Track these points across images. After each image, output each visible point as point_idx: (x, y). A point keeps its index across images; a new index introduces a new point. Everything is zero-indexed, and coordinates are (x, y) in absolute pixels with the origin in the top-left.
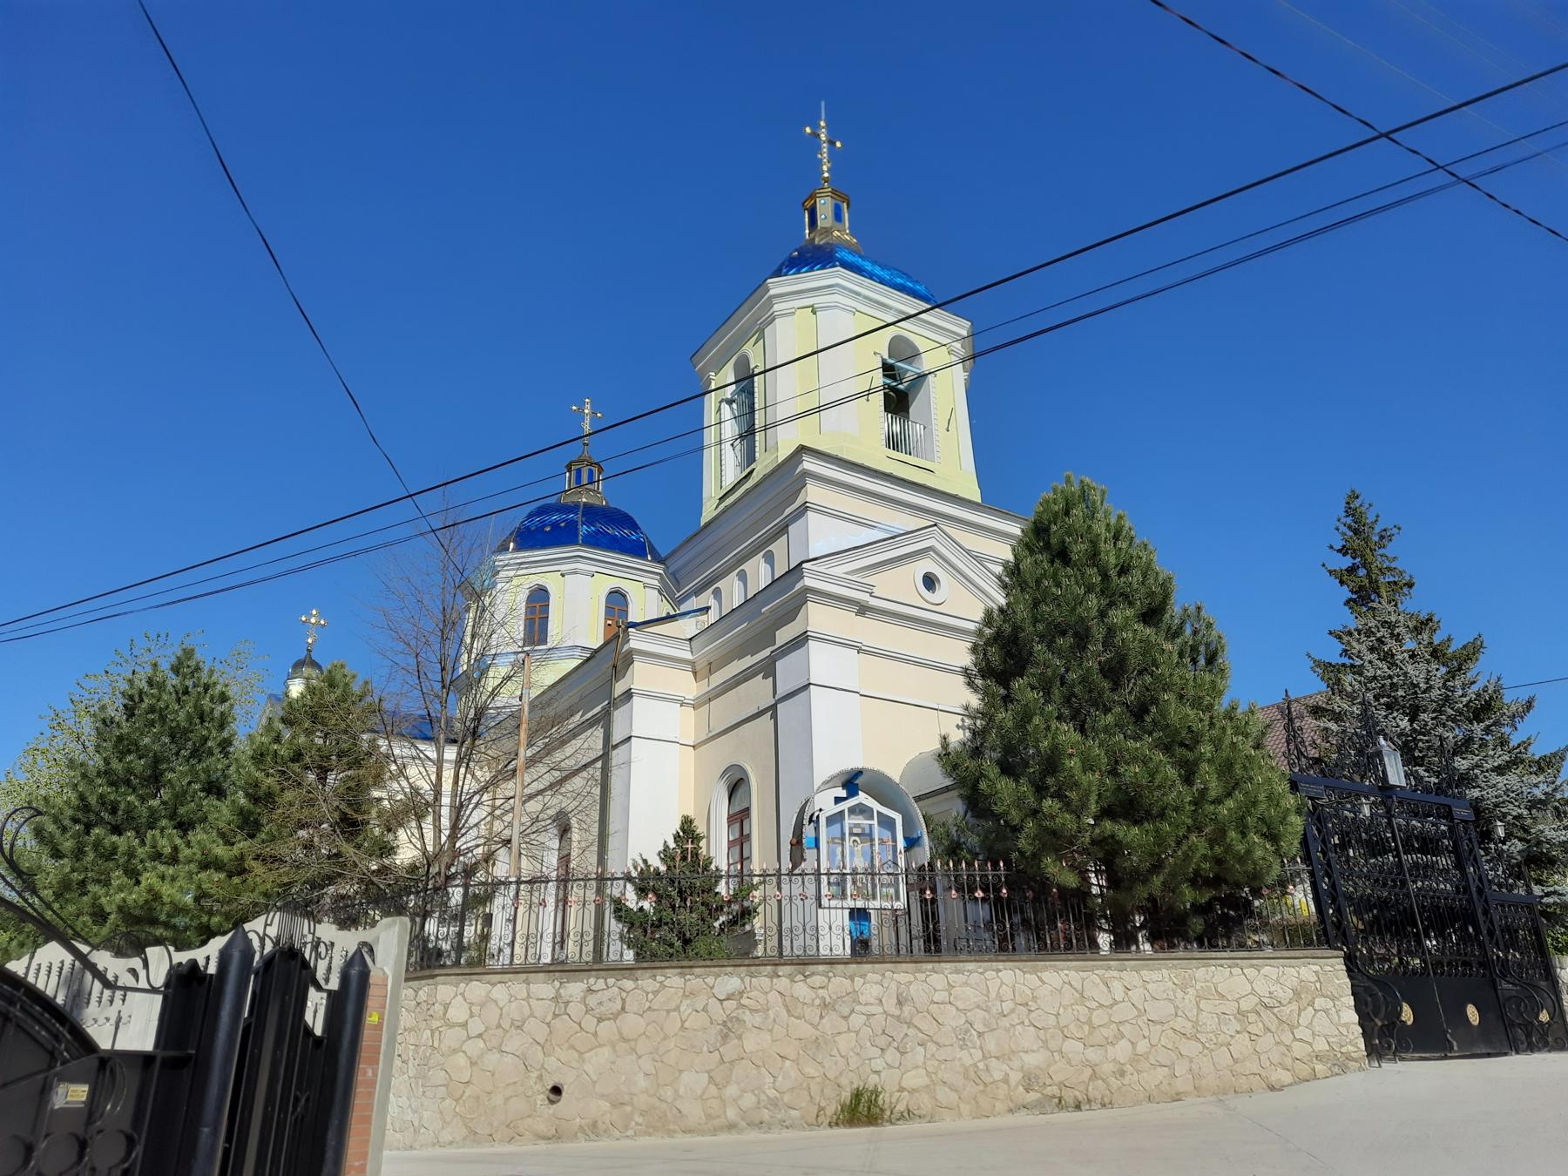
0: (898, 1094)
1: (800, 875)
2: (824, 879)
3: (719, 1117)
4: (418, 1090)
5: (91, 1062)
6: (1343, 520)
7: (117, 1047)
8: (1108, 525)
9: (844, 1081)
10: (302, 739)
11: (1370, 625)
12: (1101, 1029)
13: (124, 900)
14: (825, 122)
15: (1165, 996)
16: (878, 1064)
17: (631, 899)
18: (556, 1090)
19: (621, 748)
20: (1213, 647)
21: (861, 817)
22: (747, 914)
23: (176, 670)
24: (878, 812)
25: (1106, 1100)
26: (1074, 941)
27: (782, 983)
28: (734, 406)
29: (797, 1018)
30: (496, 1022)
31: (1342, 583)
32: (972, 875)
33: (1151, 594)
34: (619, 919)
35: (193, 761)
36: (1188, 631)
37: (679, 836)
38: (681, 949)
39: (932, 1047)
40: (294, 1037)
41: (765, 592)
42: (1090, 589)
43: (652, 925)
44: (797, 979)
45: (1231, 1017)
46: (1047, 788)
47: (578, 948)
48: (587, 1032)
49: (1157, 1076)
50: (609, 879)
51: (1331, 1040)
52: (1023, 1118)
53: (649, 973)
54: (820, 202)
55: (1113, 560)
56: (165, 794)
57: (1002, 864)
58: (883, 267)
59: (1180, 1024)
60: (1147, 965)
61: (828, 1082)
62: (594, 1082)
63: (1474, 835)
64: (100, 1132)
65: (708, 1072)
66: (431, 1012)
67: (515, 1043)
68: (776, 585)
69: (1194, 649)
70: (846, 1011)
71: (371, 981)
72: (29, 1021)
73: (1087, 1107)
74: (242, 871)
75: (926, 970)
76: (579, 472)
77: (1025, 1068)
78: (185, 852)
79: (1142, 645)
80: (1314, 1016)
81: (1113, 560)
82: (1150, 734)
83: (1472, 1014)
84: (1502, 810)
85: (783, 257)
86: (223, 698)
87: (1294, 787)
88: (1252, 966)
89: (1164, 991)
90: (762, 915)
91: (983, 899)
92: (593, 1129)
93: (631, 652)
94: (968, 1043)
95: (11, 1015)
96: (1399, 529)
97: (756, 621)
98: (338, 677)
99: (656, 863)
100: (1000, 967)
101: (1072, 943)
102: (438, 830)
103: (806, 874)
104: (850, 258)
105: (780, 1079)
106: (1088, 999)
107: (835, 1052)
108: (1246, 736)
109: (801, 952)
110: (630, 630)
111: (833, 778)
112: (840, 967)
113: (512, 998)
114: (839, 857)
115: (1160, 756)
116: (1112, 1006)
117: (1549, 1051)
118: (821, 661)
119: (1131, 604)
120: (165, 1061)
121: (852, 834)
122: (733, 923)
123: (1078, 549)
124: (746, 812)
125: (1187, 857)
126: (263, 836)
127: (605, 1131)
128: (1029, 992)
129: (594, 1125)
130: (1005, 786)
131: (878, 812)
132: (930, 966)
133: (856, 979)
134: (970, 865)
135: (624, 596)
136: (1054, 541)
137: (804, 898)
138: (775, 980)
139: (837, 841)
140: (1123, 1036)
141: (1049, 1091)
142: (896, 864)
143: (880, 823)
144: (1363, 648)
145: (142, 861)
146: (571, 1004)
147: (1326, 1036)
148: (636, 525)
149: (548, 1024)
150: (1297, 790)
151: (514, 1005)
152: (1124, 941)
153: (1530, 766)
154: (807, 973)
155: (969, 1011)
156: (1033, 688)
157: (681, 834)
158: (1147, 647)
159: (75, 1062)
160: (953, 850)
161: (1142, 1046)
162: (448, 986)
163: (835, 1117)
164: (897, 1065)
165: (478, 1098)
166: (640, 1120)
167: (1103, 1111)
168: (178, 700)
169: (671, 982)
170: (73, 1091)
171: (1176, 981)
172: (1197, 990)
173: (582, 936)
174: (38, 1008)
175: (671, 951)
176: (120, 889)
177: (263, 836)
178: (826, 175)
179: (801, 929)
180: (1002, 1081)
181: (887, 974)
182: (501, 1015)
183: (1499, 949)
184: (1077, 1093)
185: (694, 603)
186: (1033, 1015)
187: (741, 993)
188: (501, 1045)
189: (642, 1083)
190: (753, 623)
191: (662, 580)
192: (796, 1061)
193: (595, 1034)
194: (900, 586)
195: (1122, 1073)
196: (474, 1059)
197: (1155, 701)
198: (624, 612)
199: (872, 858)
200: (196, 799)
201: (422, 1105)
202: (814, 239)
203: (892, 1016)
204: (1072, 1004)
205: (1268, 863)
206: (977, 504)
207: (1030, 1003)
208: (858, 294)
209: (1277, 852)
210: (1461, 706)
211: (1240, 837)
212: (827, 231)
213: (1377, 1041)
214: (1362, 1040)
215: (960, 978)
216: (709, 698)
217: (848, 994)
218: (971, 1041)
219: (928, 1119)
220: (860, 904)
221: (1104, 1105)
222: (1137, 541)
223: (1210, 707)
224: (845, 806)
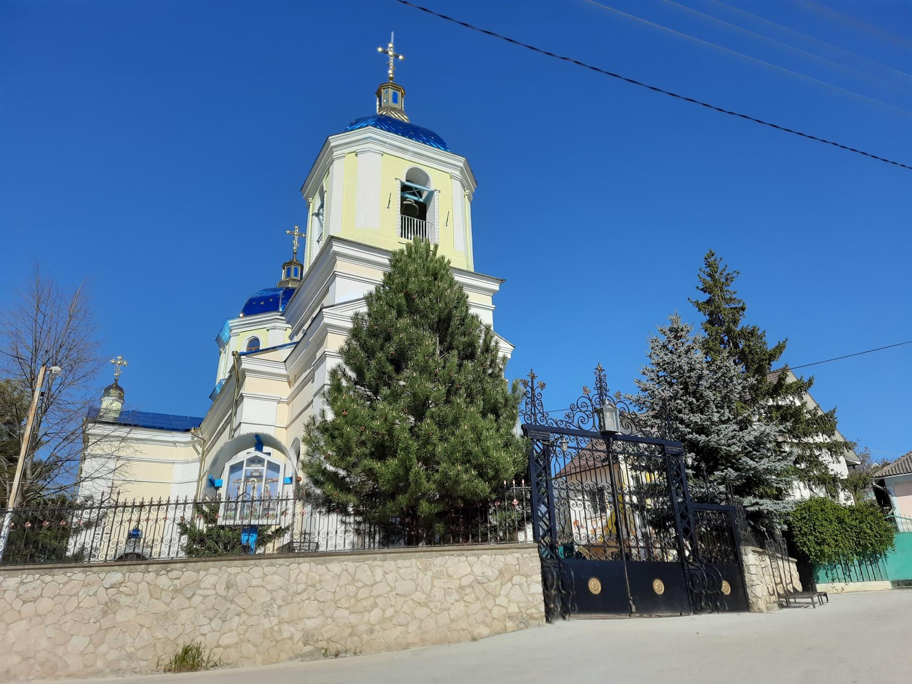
15: (410, 577)
21: (259, 465)
25: (358, 650)
27: (150, 577)
29: (156, 599)
44: (161, 573)
49: (394, 633)
52: (297, 663)
53: (62, 571)
77: (305, 630)
80: (512, 588)
88: (474, 555)
93: (244, 371)
96: (738, 273)
100: (301, 561)
110: (242, 357)
116: (373, 585)
147: (517, 603)
154: (168, 569)
155: (275, 591)
166: (38, 668)
178: (391, 76)
179: (160, 541)
186: (318, 593)
189: (44, 644)
193: (19, 612)
203: (221, 596)
204: (346, 585)
208: (385, 143)
215: (274, 569)
221: (355, 654)
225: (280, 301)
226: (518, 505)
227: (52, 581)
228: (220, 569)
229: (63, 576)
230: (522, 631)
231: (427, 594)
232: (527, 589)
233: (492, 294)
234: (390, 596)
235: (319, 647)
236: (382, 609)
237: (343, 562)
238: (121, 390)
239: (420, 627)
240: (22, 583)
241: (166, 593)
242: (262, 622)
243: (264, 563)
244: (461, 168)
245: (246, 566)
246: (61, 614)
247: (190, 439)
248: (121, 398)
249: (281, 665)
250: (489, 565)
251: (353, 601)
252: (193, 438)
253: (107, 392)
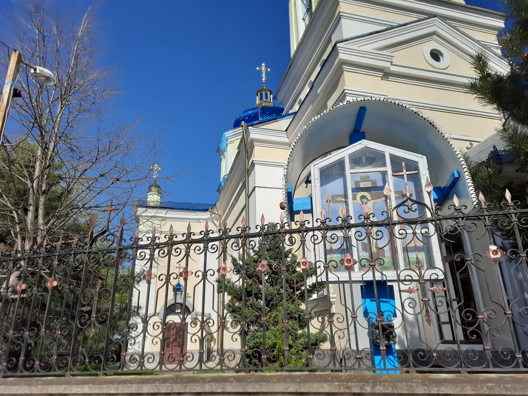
93: (252, 141)
110: (249, 128)
121: (357, 189)
139: (339, 199)
225: (259, 115)
226: (4, 289)
233: (496, 32)
238: (158, 187)
247: (209, 216)
248: (159, 193)
252: (211, 216)
253: (150, 190)
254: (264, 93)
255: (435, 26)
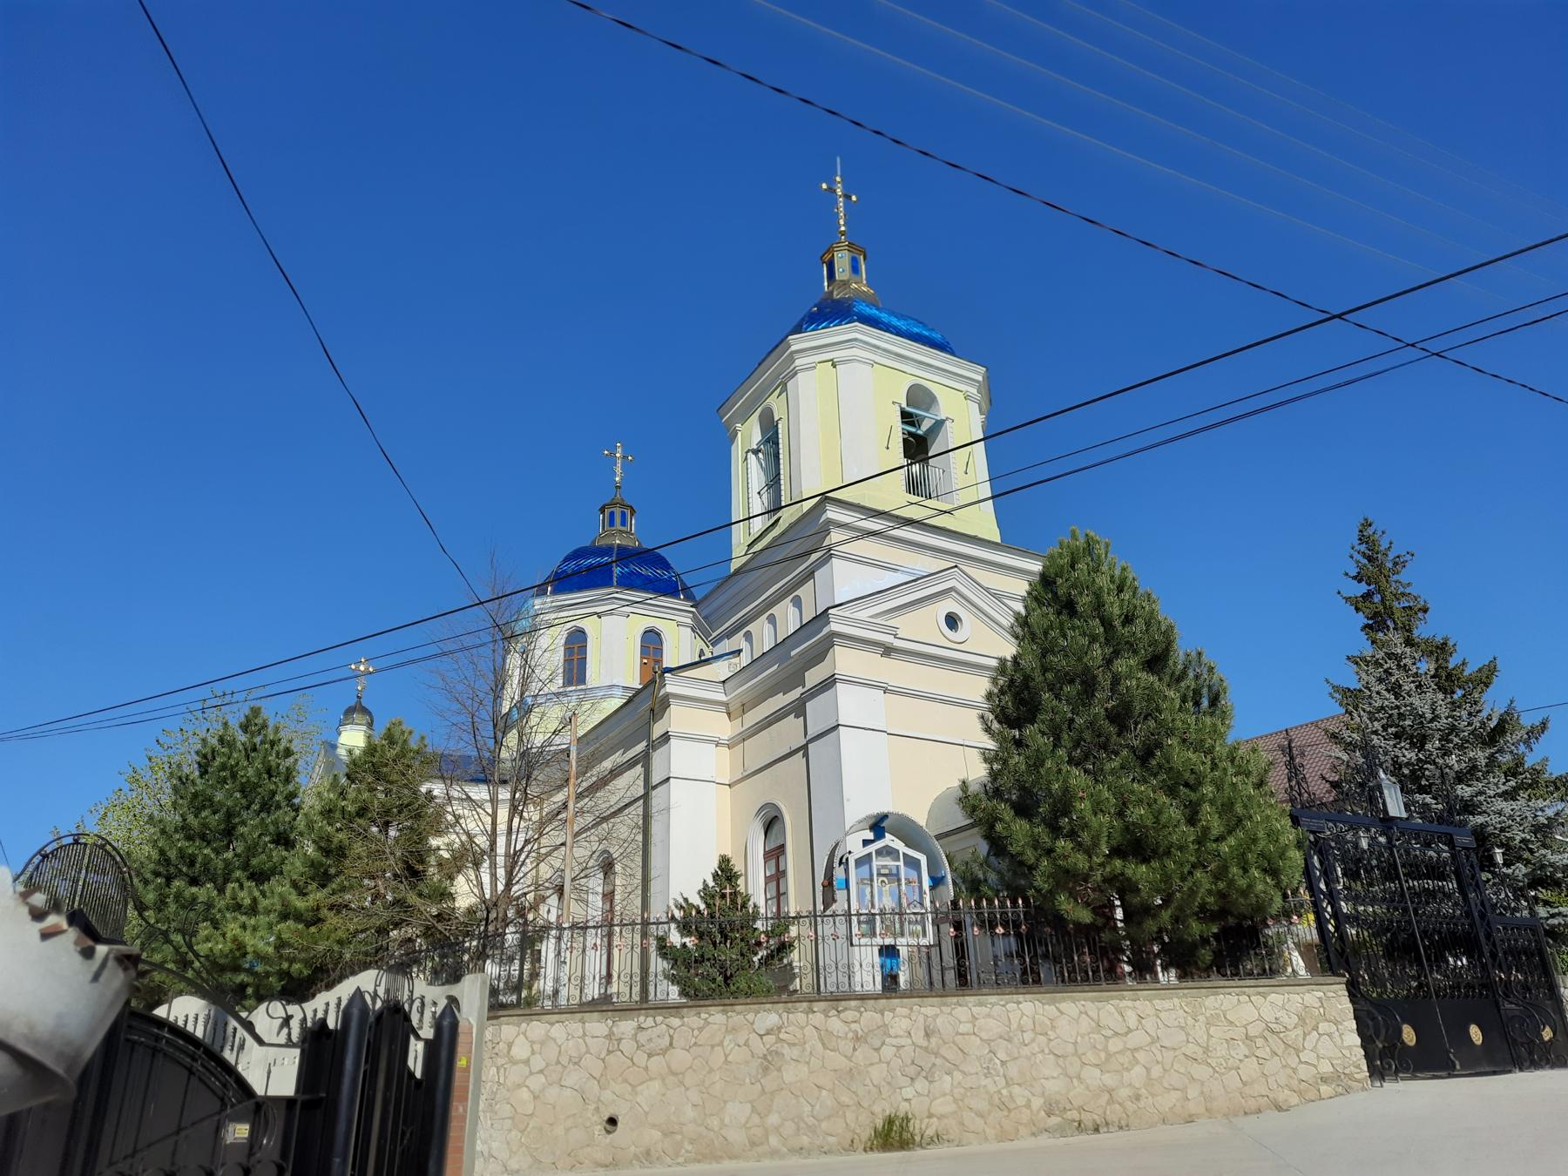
0: (927, 1120)
1: (831, 916)
2: (854, 919)
3: (762, 1144)
4: (486, 1123)
5: (250, 1104)
6: (1357, 548)
7: (269, 1094)
8: (1112, 577)
9: (877, 1109)
10: (366, 795)
11: (1377, 656)
12: (1117, 1055)
13: (211, 950)
14: (841, 176)
15: (1176, 1023)
16: (908, 1092)
17: (675, 938)
18: (612, 1121)
19: (659, 789)
20: (1215, 688)
21: (888, 858)
22: (784, 948)
23: (245, 728)
24: (904, 854)
25: (1123, 1123)
26: (1090, 973)
27: (817, 1018)
28: (760, 455)
29: (831, 1050)
30: (555, 1060)
31: (1357, 609)
32: (992, 913)
33: (1153, 643)
34: (664, 956)
35: (263, 815)
36: (1191, 674)
37: (718, 875)
38: (722, 984)
39: (958, 1075)
40: (401, 1077)
41: (794, 637)
42: (1094, 639)
43: (696, 961)
44: (830, 1014)
45: (1240, 1043)
46: (1060, 828)
47: (628, 988)
48: (639, 1067)
49: (1169, 1100)
50: (654, 923)
51: (1334, 1062)
52: (1044, 1141)
53: (694, 1011)
54: (837, 256)
55: (1116, 611)
56: (239, 846)
57: (1020, 902)
58: (900, 317)
59: (1191, 1049)
60: (1159, 995)
61: (862, 1110)
62: (647, 1114)
63: (1475, 861)
64: (259, 1162)
65: (750, 1102)
66: (496, 1050)
67: (573, 1078)
68: (804, 629)
69: (1197, 693)
70: (877, 1043)
71: (460, 1030)
72: (208, 1074)
73: (1105, 1129)
74: (318, 921)
75: (951, 1004)
76: (612, 514)
77: (1046, 1094)
78: (264, 903)
79: (1146, 692)
80: (1319, 1039)
81: (1116, 611)
82: (1155, 776)
83: (1476, 1034)
84: (1507, 834)
85: (801, 313)
86: (288, 753)
87: (1295, 821)
88: (1259, 994)
89: (1176, 1019)
90: (797, 950)
91: (1003, 934)
92: (647, 1156)
93: (667, 696)
94: (992, 1071)
95: (194, 1070)
96: (1413, 555)
97: (786, 664)
98: (397, 734)
99: (696, 900)
100: (1021, 1000)
101: (1088, 975)
102: (494, 876)
103: (837, 915)
104: (873, 312)
105: (817, 1107)
106: (1104, 1028)
107: (868, 1081)
108: (1248, 774)
109: (834, 989)
110: (666, 675)
111: (860, 822)
112: (871, 1002)
113: (569, 1037)
114: (869, 897)
115: (1163, 799)
116: (1127, 1034)
117: (1552, 1067)
118: (849, 703)
119: (1135, 652)
120: (306, 1105)
121: (879, 874)
122: (771, 956)
123: (1084, 601)
124: (781, 849)
125: (1192, 892)
126: (334, 886)
127: (658, 1159)
128: (1048, 1023)
129: (648, 1153)
130: (1020, 827)
131: (904, 854)
132: (955, 1000)
133: (886, 1013)
134: (990, 902)
135: (658, 635)
136: (1060, 592)
137: (835, 937)
138: (810, 1016)
139: (865, 882)
140: (1137, 1062)
141: (1069, 1115)
142: (921, 904)
143: (906, 864)
144: (1372, 680)
145: (219, 911)
146: (623, 1041)
147: (1330, 1059)
148: (669, 564)
149: (603, 1060)
150: (1299, 825)
151: (571, 1042)
152: (1143, 969)
153: (1547, 786)
154: (840, 1009)
155: (993, 1041)
156: (1043, 733)
157: (720, 873)
158: (1151, 695)
159: (240, 1106)
160: (972, 885)
161: (1156, 1072)
162: (511, 1026)
163: (869, 1144)
164: (926, 1091)
165: (541, 1129)
166: (689, 1148)
167: (1120, 1133)
168: (248, 757)
169: (715, 1018)
170: (239, 1129)
171: (1187, 1009)
172: (1206, 1018)
173: (631, 977)
174: (213, 1063)
175: (713, 986)
176: (207, 939)
177: (334, 886)
178: (843, 228)
179: (834, 968)
180: (1025, 1106)
181: (915, 1007)
182: (560, 1052)
183: (1501, 970)
184: (1096, 1117)
185: (726, 646)
186: (1052, 1043)
187: (779, 1028)
188: (560, 1079)
189: (690, 1113)
190: (784, 666)
191: (695, 618)
192: (832, 1091)
193: (646, 1069)
194: (923, 627)
195: (1138, 1098)
196: (537, 1094)
197: (1159, 745)
198: (659, 650)
199: (900, 896)
200: (267, 850)
201: (491, 1136)
202: (832, 292)
203: (921, 1047)
204: (1089, 1033)
205: (1270, 897)
206: (997, 544)
207: (1049, 1033)
208: (878, 348)
209: (1278, 885)
210: (1466, 734)
211: (1241, 872)
212: (845, 284)
213: (1379, 1063)
214: (1365, 1061)
215: (984, 1010)
216: (744, 737)
217: (879, 1028)
218: (995, 1070)
219: (956, 1143)
220: (889, 941)
221: (1121, 1128)
222: (1141, 591)
223: (1210, 751)
224: (872, 848)
227: (682, 1025)
228: (911, 1009)
229: (695, 1017)
230: (1341, 1097)
231: (1203, 1047)
232: (1340, 1041)
234: (1153, 1049)
235: (1070, 1118)
236: (1145, 1067)
237: (1078, 1001)
239: (1202, 1093)
240: (640, 1028)
241: (843, 1042)
242: (983, 1083)
243: (970, 1002)
244: (978, 382)
245: (945, 1004)
246: (704, 1073)
249: (1016, 1144)
250: (1283, 1007)
251: (1103, 1055)
254: (618, 511)
255: (954, 580)
